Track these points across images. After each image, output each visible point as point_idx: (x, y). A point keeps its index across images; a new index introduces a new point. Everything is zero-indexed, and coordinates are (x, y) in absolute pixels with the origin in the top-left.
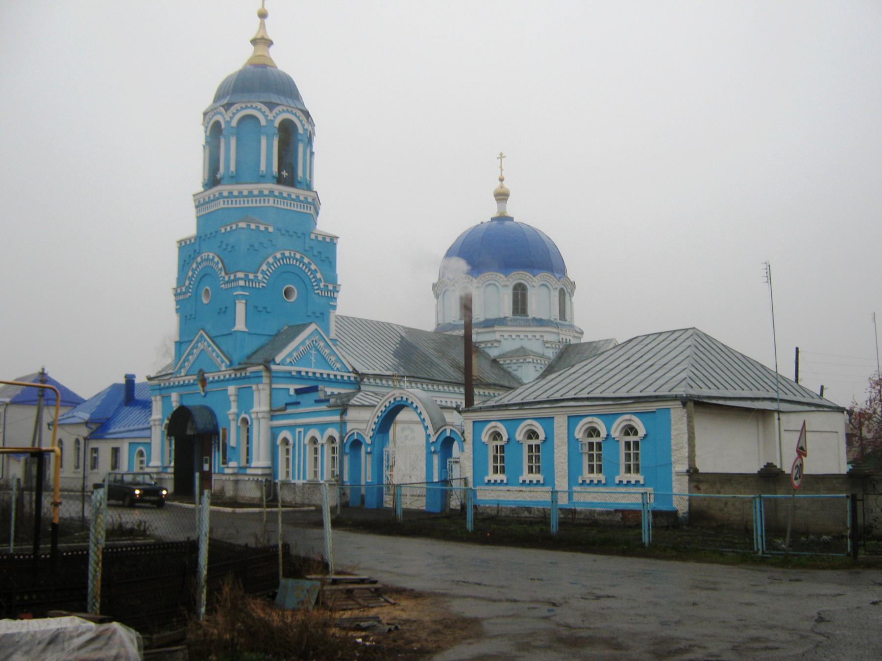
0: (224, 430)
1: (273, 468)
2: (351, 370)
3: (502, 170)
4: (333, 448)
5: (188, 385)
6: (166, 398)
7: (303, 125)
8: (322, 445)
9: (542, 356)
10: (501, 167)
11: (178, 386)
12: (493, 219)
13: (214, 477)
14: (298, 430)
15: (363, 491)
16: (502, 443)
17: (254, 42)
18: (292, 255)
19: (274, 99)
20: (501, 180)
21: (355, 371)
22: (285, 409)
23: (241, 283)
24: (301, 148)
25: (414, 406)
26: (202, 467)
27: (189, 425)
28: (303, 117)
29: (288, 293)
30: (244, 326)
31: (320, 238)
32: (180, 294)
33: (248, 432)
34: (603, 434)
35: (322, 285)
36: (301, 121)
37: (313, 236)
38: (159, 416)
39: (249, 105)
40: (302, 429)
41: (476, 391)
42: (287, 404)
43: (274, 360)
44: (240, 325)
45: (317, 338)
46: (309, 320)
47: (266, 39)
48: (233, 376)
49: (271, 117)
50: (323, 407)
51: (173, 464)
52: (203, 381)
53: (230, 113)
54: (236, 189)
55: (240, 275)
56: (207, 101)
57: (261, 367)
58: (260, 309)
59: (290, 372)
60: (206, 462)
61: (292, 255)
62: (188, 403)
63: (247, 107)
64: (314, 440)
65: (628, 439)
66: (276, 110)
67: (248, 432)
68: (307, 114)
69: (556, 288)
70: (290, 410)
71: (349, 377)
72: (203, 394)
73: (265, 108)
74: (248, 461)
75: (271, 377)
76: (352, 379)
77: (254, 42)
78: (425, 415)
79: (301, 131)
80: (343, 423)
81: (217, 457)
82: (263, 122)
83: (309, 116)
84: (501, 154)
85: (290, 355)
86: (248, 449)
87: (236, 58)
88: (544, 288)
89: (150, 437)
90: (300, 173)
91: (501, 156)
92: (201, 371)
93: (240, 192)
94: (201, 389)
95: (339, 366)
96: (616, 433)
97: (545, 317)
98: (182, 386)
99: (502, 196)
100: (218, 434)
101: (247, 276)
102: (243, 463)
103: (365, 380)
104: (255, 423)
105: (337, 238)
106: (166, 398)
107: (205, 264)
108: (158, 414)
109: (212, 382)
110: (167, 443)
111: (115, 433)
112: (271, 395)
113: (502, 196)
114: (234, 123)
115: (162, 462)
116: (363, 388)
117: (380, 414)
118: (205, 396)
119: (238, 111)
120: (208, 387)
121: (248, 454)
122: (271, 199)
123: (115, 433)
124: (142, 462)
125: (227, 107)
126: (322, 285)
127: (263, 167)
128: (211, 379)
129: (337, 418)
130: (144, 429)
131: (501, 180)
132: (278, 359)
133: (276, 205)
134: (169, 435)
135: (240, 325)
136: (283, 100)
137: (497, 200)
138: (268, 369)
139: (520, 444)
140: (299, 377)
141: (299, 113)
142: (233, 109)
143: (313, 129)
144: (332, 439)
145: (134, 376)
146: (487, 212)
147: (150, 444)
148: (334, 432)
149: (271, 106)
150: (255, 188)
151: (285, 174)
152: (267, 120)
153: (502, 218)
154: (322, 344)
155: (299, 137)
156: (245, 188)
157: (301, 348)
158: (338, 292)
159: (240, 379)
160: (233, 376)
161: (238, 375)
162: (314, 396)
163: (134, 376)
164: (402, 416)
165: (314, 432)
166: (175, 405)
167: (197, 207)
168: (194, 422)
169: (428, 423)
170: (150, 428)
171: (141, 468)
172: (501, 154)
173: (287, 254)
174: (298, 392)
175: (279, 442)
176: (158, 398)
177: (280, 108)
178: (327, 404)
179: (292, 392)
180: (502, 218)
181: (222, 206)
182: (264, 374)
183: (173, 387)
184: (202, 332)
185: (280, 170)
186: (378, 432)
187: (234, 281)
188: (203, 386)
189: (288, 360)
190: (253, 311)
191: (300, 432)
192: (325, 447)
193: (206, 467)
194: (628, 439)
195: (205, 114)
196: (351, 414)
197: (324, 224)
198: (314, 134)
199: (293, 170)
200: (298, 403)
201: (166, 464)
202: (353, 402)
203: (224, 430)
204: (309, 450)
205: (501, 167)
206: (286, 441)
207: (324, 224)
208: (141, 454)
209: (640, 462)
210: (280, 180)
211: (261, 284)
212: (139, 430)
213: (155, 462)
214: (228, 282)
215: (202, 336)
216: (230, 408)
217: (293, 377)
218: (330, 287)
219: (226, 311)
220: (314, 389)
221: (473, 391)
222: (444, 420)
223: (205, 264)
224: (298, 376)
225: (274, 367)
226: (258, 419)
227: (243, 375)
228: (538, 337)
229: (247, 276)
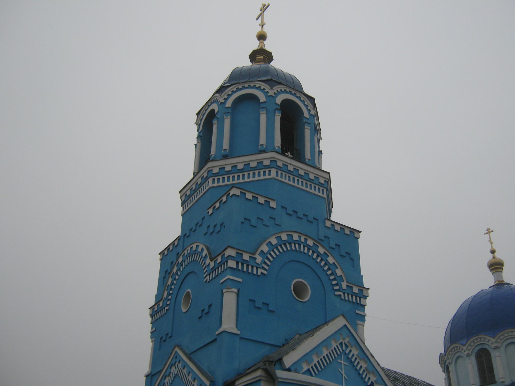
3: (492, 243)
7: (309, 111)
10: (490, 241)
17: (286, 340)
18: (303, 240)
20: (493, 252)
23: (232, 264)
24: (307, 132)
28: (307, 102)
29: (299, 290)
30: (233, 325)
31: (337, 228)
35: (344, 285)
36: (307, 106)
37: (328, 224)
43: (280, 360)
44: (229, 324)
45: (347, 340)
49: (271, 93)
54: (228, 164)
55: (230, 252)
58: (259, 304)
61: (303, 240)
63: (244, 88)
79: (306, 114)
82: (262, 98)
84: (488, 229)
91: (489, 232)
93: (234, 167)
99: (496, 266)
101: (239, 254)
105: (360, 232)
113: (496, 266)
114: (229, 104)
119: (233, 92)
122: (273, 171)
126: (344, 285)
127: (263, 140)
131: (493, 252)
132: (289, 360)
133: (279, 178)
135: (229, 324)
137: (491, 270)
146: (486, 281)
150: (253, 160)
152: (268, 97)
153: (500, 284)
154: (355, 352)
156: (240, 162)
157: (325, 352)
158: (366, 297)
172: (488, 229)
173: (296, 237)
180: (500, 284)
181: (211, 185)
184: (177, 349)
189: (305, 368)
190: (248, 306)
197: (340, 215)
205: (490, 241)
207: (340, 215)
211: (260, 271)
214: (214, 269)
215: (176, 356)
218: (355, 290)
219: (211, 311)
225: (280, 374)
229: (239, 254)
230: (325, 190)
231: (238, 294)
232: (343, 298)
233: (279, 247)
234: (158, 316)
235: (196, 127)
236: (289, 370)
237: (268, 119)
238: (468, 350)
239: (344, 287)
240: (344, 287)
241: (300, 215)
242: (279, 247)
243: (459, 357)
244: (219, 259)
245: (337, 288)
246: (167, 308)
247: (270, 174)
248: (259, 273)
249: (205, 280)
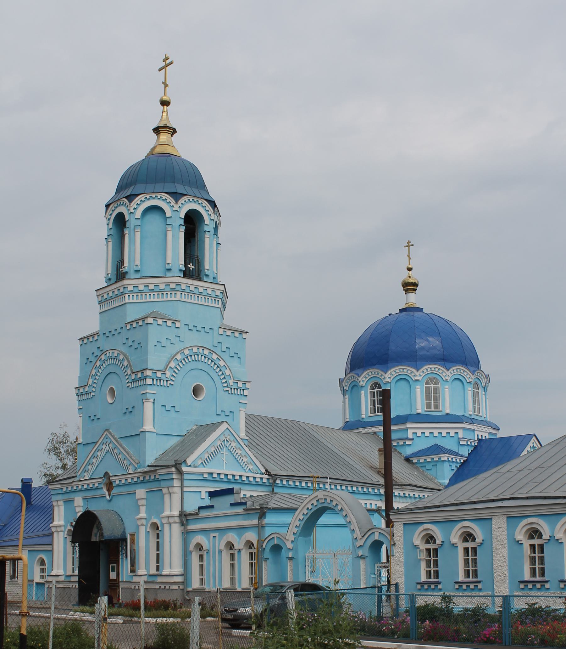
0: (132, 535)
1: (186, 573)
2: (263, 471)
4: (251, 554)
5: (92, 489)
6: (69, 502)
8: (239, 551)
9: (457, 454)
11: (81, 490)
12: (401, 310)
13: (121, 586)
14: (212, 535)
15: (24, 632)
16: (434, 546)
19: (180, 189)
21: (268, 473)
22: (197, 514)
25: (339, 508)
26: (108, 575)
27: (95, 530)
28: (209, 207)
30: (152, 427)
32: (82, 394)
33: (158, 538)
34: (545, 536)
38: (62, 523)
39: (154, 196)
40: (217, 534)
41: (396, 492)
42: (200, 508)
43: (185, 461)
46: (219, 419)
47: (169, 128)
48: (141, 479)
49: (176, 208)
50: (240, 510)
51: (77, 572)
52: (110, 486)
53: (134, 204)
56: (110, 192)
57: (173, 469)
59: (202, 474)
60: (113, 570)
62: (93, 507)
64: (230, 546)
65: (532, 542)
66: (182, 200)
67: (158, 538)
68: (213, 204)
69: (470, 383)
70: (203, 514)
71: (262, 479)
72: (108, 497)
73: (169, 198)
74: (158, 569)
75: (182, 480)
76: (265, 480)
77: (157, 130)
78: (351, 517)
79: (207, 220)
80: (261, 527)
81: (125, 565)
83: (215, 206)
84: (409, 242)
85: (199, 457)
86: (158, 555)
87: (138, 147)
88: (458, 382)
89: (51, 544)
90: (207, 266)
92: (106, 474)
94: (107, 493)
95: (251, 467)
96: (455, 539)
97: (460, 413)
98: (86, 490)
100: (125, 540)
102: (153, 571)
103: (278, 481)
104: (166, 527)
106: (69, 502)
107: (109, 362)
108: (62, 520)
109: (118, 486)
110: (70, 549)
111: (9, 541)
112: (182, 498)
115: (65, 570)
116: (276, 490)
117: (301, 517)
118: (110, 501)
120: (114, 491)
121: (158, 561)
123: (9, 541)
124: (42, 571)
125: (130, 198)
128: (117, 482)
129: (255, 522)
130: (44, 536)
132: (189, 461)
134: (73, 542)
136: (188, 190)
138: (180, 472)
139: (454, 546)
140: (211, 478)
141: (205, 203)
142: (137, 200)
143: (219, 220)
144: (250, 545)
145: (31, 480)
147: (52, 551)
148: (252, 536)
149: (177, 196)
151: (191, 266)
155: (206, 228)
159: (148, 482)
160: (141, 479)
161: (147, 478)
162: (230, 499)
163: (31, 480)
164: (324, 519)
165: (232, 537)
166: (80, 511)
167: (100, 302)
168: (100, 528)
169: (354, 526)
170: (51, 535)
171: (42, 577)
172: (409, 242)
174: (212, 494)
175: (191, 547)
176: (61, 503)
177: (186, 198)
178: (244, 507)
179: (205, 495)
182: (174, 476)
183: (76, 491)
185: (186, 264)
186: (299, 536)
187: (140, 379)
188: (109, 490)
189: (200, 462)
191: (215, 537)
192: (243, 552)
193: (113, 576)
194: (532, 542)
195: (107, 206)
196: (270, 519)
198: (220, 224)
199: (199, 262)
200: (212, 507)
201: (70, 573)
202: (272, 505)
203: (132, 535)
204: (226, 556)
206: (199, 547)
208: (42, 562)
209: (547, 566)
210: (187, 274)
212: (38, 537)
213: (58, 570)
216: (138, 512)
217: (205, 480)
220: (230, 492)
221: (392, 493)
222: (371, 522)
223: (109, 362)
224: (210, 478)
225: (184, 469)
226: (170, 524)
227: (153, 477)
228: (452, 434)
230: (220, 300)
231: (154, 403)
232: (230, 392)
233: (183, 361)
234: (84, 397)
235: (106, 221)
236: (190, 466)
237: (173, 236)
238: (365, 378)
239: (231, 384)
240: (231, 384)
241: (199, 328)
242: (183, 361)
243: (355, 385)
244: (139, 375)
245: (226, 385)
246: (92, 394)
247: (175, 297)
248: (168, 385)
249: (128, 385)
